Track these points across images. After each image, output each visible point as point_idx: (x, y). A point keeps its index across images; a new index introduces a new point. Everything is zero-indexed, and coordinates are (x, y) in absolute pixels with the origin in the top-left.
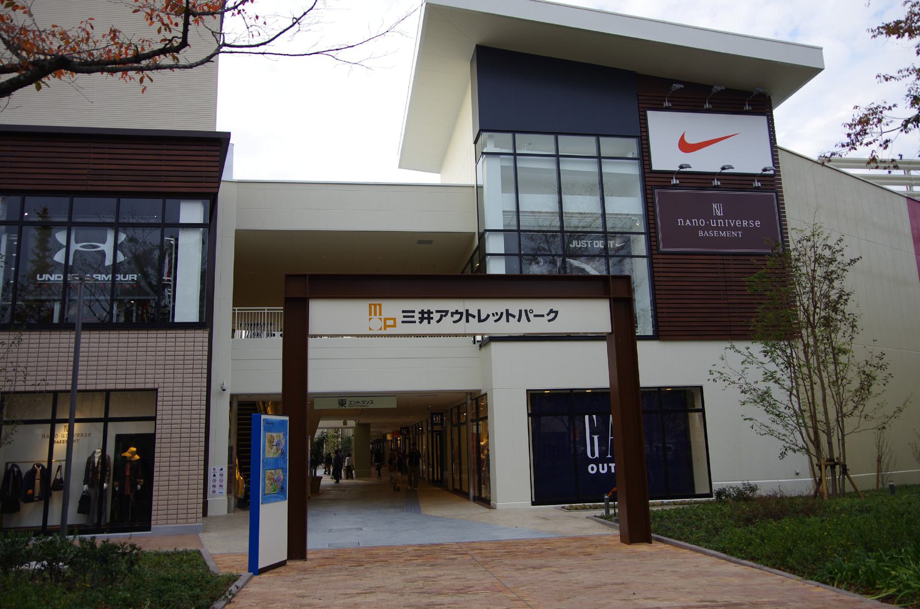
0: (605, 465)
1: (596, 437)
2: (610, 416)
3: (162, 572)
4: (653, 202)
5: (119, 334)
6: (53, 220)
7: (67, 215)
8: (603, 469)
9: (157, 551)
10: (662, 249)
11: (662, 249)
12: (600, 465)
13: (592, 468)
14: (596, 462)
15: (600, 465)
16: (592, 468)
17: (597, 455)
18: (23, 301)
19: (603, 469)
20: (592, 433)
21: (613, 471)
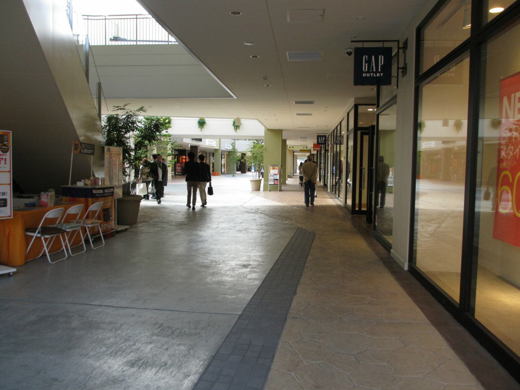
0: (369, 74)
1: (367, 64)
2: (372, 57)
3: (150, 374)
4: (7, 138)
5: (88, 19)
6: (77, 39)
7: (139, 214)
8: (368, 75)
9: (316, 183)
10: (11, 132)
11: (11, 132)
12: (367, 74)
13: (364, 75)
14: (366, 73)
15: (367, 74)
16: (364, 75)
17: (366, 70)
18: (207, 238)
19: (368, 75)
20: (365, 63)
21: (382, 75)
